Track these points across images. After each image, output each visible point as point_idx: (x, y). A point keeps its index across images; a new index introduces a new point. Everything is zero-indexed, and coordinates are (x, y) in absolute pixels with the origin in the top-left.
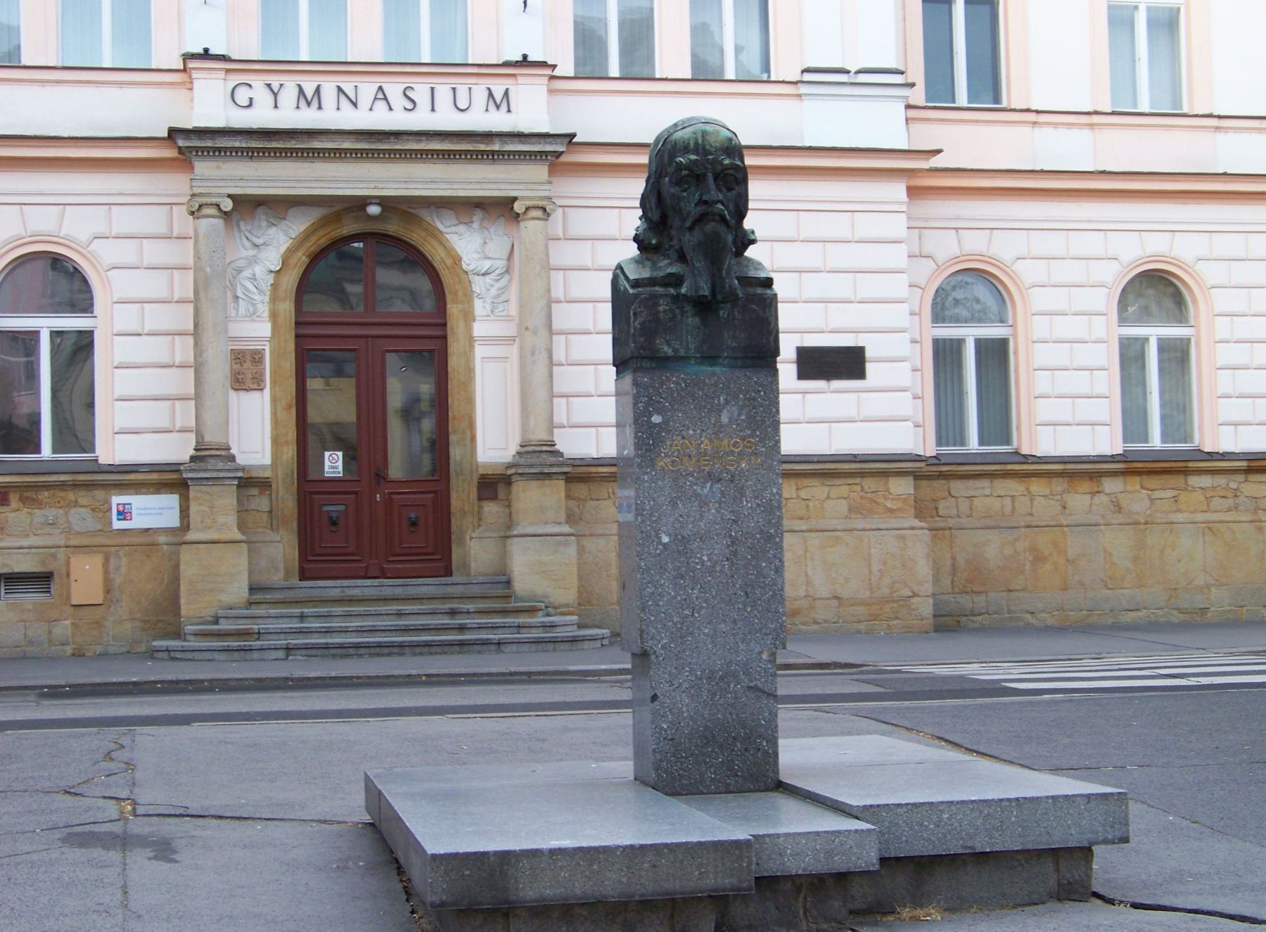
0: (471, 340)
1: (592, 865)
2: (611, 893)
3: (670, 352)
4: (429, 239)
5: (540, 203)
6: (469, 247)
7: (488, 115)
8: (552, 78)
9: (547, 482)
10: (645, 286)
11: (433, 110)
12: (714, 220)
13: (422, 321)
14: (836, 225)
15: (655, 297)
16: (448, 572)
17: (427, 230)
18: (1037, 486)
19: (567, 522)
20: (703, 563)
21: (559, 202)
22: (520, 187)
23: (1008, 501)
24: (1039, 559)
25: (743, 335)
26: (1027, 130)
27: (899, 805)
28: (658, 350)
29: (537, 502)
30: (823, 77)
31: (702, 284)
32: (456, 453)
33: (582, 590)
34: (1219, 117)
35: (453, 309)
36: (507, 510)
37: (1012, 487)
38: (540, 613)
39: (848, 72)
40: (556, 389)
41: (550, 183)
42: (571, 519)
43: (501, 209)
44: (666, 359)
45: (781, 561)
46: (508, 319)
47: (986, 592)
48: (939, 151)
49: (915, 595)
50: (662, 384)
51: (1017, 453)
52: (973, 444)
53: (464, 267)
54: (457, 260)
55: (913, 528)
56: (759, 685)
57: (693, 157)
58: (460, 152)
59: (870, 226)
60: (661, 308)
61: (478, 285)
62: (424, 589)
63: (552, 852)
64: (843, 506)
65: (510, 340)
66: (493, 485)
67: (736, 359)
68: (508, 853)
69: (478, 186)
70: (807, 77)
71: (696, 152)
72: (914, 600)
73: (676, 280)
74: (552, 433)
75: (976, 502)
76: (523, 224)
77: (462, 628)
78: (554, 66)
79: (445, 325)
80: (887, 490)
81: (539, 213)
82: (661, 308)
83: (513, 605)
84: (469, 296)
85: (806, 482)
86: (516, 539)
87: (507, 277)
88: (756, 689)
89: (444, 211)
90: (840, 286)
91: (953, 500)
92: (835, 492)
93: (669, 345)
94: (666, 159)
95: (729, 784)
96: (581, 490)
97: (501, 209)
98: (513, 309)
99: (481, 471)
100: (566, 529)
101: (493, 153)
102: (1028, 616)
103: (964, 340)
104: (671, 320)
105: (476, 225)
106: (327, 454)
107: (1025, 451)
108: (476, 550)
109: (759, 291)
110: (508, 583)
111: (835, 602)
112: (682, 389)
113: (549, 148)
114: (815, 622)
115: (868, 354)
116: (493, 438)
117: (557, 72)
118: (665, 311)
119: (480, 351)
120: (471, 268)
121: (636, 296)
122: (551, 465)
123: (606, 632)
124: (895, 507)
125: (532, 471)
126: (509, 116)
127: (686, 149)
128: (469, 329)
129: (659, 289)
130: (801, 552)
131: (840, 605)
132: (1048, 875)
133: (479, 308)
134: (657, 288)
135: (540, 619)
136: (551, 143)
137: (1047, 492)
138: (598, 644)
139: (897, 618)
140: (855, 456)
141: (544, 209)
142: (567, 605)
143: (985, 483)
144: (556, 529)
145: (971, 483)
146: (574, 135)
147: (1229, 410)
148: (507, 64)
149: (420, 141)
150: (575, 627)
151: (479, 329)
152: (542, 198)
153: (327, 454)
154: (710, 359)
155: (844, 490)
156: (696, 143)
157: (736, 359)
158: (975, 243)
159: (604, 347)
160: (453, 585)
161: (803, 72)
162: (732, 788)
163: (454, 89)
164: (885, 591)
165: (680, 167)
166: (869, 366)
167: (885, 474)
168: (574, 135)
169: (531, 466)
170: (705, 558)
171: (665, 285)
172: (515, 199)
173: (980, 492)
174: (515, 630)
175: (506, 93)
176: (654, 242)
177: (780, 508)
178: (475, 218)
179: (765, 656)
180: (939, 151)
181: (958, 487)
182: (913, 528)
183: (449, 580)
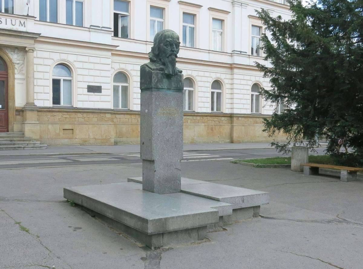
0: (14, 78)
1: (185, 220)
2: (189, 226)
3: (161, 87)
4: (4, 54)
5: (32, 49)
6: (14, 57)
7: (20, 27)
8: (35, 20)
9: (33, 112)
11: (6, 24)
12: (174, 55)
13: (3, 73)
14: (97, 60)
15: (157, 73)
16: (8, 131)
17: (4, 52)
18: (133, 117)
19: (37, 121)
20: (166, 138)
21: (36, 49)
22: (28, 45)
23: (127, 119)
24: (133, 131)
26: (134, 44)
27: (228, 198)
28: (158, 86)
29: (31, 116)
30: (93, 28)
32: (10, 104)
33: (40, 136)
35: (10, 71)
36: (22, 118)
37: (128, 116)
38: (31, 141)
39: (100, 27)
40: (35, 91)
41: (34, 44)
42: (38, 120)
43: (23, 50)
44: (160, 88)
45: (183, 138)
46: (23, 74)
47: (123, 138)
48: (119, 46)
49: (111, 138)
51: (129, 110)
52: (120, 107)
53: (13, 62)
54: (11, 61)
55: (110, 124)
56: (177, 168)
57: (171, 39)
58: (13, 35)
59: (104, 61)
61: (16, 66)
62: (2, 135)
63: (177, 217)
64: (96, 119)
65: (24, 79)
66: (21, 111)
67: (174, 89)
68: (167, 218)
69: (17, 43)
70: (92, 27)
72: (111, 139)
73: (162, 70)
74: (34, 101)
75: (121, 119)
76: (28, 53)
77: (14, 144)
78: (36, 18)
79: (7, 75)
80: (106, 116)
81: (32, 51)
82: (159, 76)
83: (25, 139)
84: (14, 69)
85: (88, 114)
86: (26, 124)
87: (23, 65)
88: (177, 168)
89: (8, 48)
90: (97, 73)
91: (116, 119)
92: (95, 116)
93: (161, 85)
94: (163, 38)
95: (170, 191)
96: (40, 113)
97: (23, 50)
98: (24, 72)
99: (16, 109)
100: (37, 122)
101: (21, 36)
102: (131, 143)
103: (119, 86)
105: (16, 52)
107: (131, 109)
108: (15, 127)
110: (23, 134)
111: (95, 139)
113: (35, 36)
114: (90, 143)
115: (102, 88)
116: (19, 101)
117: (36, 19)
119: (16, 81)
120: (14, 62)
121: (154, 72)
122: (34, 108)
123: (46, 145)
124: (107, 120)
125: (30, 109)
126: (24, 28)
127: (169, 37)
128: (14, 76)
130: (88, 129)
131: (95, 140)
132: (252, 212)
133: (16, 71)
134: (158, 71)
135: (31, 142)
136: (35, 35)
137: (135, 118)
138: (45, 148)
139: (107, 143)
140: (99, 109)
141: (33, 50)
142: (37, 139)
143: (123, 115)
144: (35, 122)
145: (120, 115)
146: (41, 34)
147: (201, 105)
148: (23, 16)
149: (4, 31)
150: (39, 144)
151: (17, 76)
152: (32, 48)
155: (97, 116)
156: (171, 36)
157: (174, 89)
158: (123, 66)
159: (139, 85)
160: (10, 134)
161: (90, 26)
162: (171, 192)
163: (11, 20)
164: (104, 137)
165: (167, 41)
166: (102, 90)
167: (105, 113)
168: (41, 34)
169: (29, 108)
170: (167, 137)
171: (160, 70)
172: (26, 47)
173: (122, 117)
174: (27, 145)
175: (24, 23)
176: (155, 59)
177: (183, 126)
178: (15, 51)
179: (179, 161)
180: (119, 46)
181: (118, 116)
182: (110, 124)
183: (8, 133)
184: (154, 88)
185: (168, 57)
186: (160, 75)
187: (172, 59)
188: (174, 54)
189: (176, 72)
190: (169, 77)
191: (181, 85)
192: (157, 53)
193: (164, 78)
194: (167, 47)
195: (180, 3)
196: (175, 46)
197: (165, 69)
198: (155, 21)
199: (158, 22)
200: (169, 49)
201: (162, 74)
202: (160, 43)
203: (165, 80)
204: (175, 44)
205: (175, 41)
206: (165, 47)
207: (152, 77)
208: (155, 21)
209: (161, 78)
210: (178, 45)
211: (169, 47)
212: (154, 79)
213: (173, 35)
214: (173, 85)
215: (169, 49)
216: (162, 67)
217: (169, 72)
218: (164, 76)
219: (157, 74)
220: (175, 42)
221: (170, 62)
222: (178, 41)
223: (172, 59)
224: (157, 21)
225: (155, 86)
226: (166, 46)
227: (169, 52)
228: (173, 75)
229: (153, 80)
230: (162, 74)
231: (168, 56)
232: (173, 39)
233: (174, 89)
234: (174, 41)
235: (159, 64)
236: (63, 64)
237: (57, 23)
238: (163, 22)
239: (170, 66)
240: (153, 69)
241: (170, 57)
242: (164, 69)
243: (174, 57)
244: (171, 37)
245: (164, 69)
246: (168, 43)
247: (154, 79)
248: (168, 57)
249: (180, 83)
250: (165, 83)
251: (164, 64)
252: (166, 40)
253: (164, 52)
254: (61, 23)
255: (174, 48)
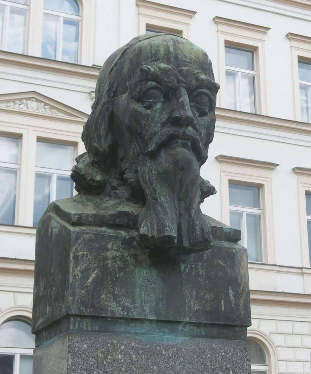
3: (119, 312)
10: (89, 224)
12: (184, 146)
15: (100, 237)
25: (208, 296)
31: (168, 222)
34: (279, 266)
44: (114, 320)
50: (106, 354)
57: (163, 65)
60: (109, 254)
67: (198, 325)
71: (168, 61)
73: (127, 222)
82: (109, 254)
93: (118, 302)
104: (121, 269)
106: (249, 335)
109: (226, 244)
112: (218, 353)
118: (114, 258)
121: (78, 236)
129: (109, 232)
134: (104, 229)
153: (249, 335)
154: (167, 323)
157: (198, 325)
165: (147, 76)
176: (98, 178)
184: (82, 316)
185: (153, 155)
186: (113, 251)
187: (175, 162)
188: (186, 137)
189: (198, 228)
190: (164, 255)
191: (237, 305)
192: (104, 145)
193: (138, 263)
194: (149, 107)
195: (298, 171)
196: (185, 98)
197: (140, 218)
198: (241, 214)
199: (248, 215)
200: (158, 113)
201: (127, 243)
202: (115, 95)
203: (143, 276)
204: (190, 92)
205: (187, 75)
206: (139, 107)
207: (68, 256)
208: (241, 214)
209: (120, 263)
210: (204, 93)
211: (159, 106)
212: (82, 266)
213: (175, 49)
214: (193, 303)
215: (158, 113)
216: (129, 208)
217: (161, 227)
218: (135, 256)
219: (97, 247)
220: (186, 77)
221: (166, 177)
222: (203, 77)
223: (175, 162)
224: (247, 214)
225: (83, 303)
226: (139, 100)
227: (157, 129)
228: (186, 243)
229: (75, 272)
230: (127, 243)
231: (152, 147)
232: (178, 66)
233: (194, 320)
234: (181, 71)
235: (117, 197)
236: (20, 318)
237: (13, 226)
238: (260, 216)
239: (164, 198)
240: (75, 219)
241: (163, 154)
242: (136, 217)
243: (183, 152)
244: (167, 58)
245: (136, 217)
246: (154, 84)
247: (82, 266)
248: (153, 155)
249: (231, 293)
250: (145, 290)
251: (138, 195)
252: (142, 70)
253: (136, 131)
254: (22, 225)
255: (182, 105)
